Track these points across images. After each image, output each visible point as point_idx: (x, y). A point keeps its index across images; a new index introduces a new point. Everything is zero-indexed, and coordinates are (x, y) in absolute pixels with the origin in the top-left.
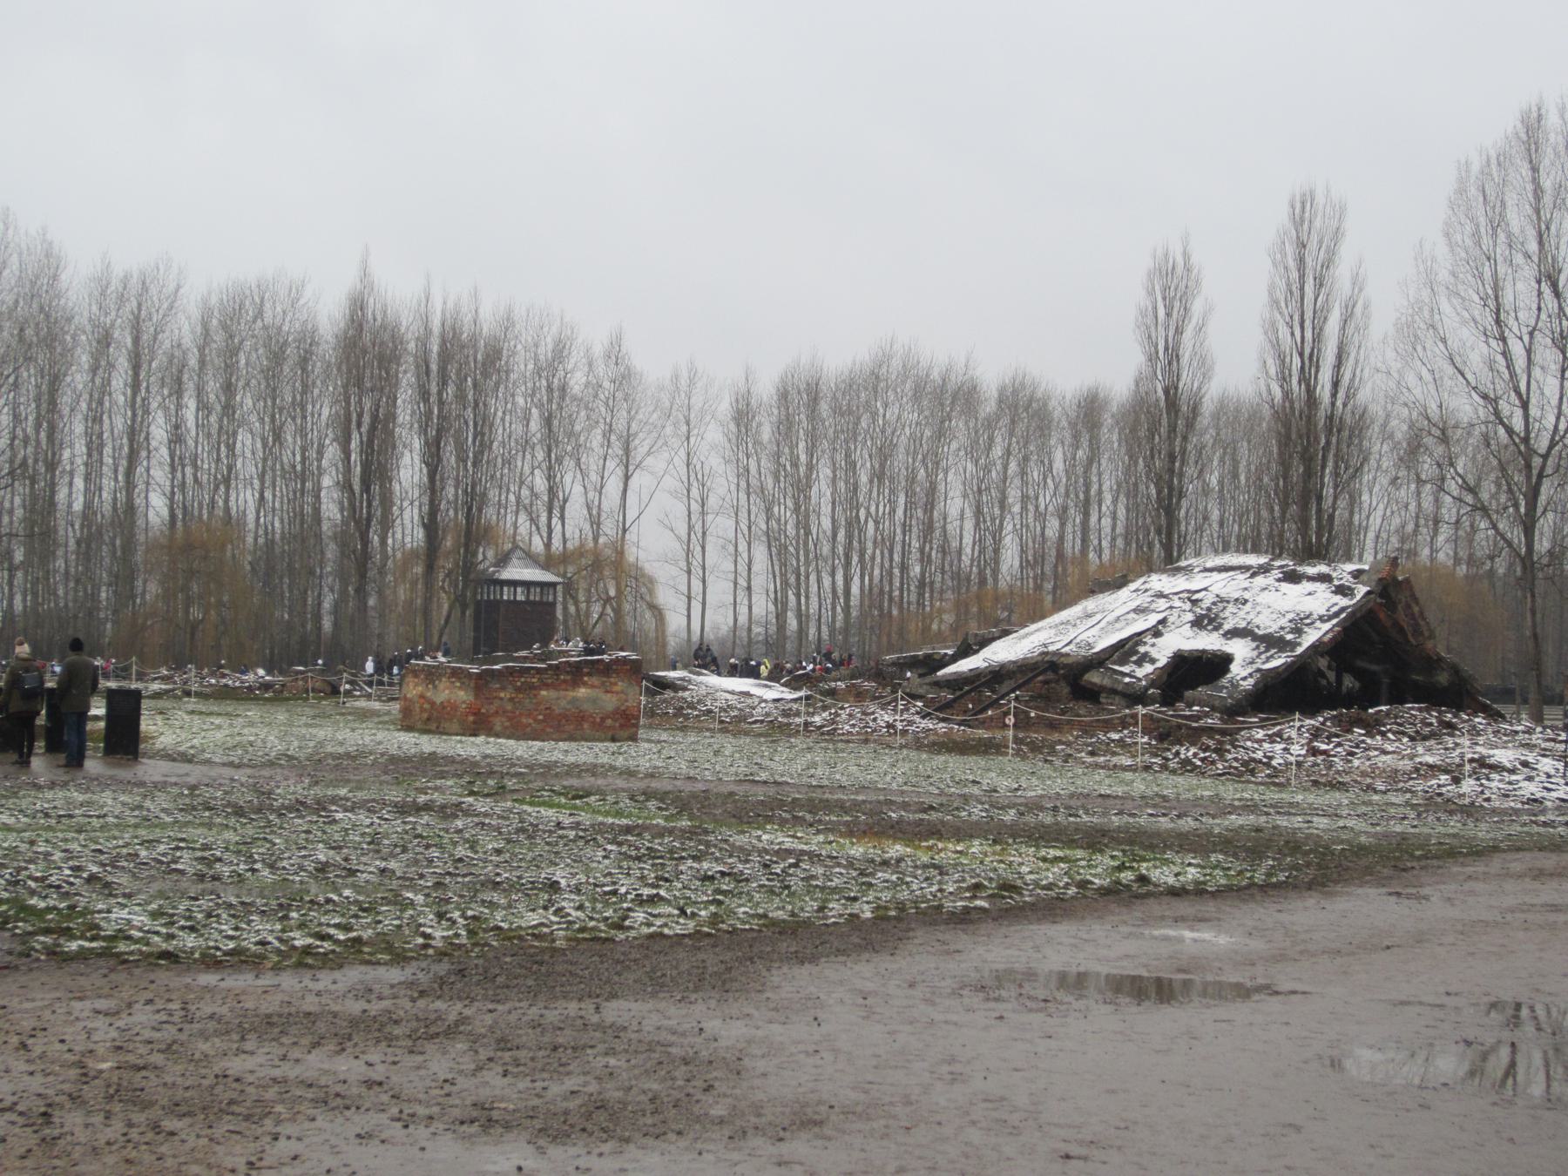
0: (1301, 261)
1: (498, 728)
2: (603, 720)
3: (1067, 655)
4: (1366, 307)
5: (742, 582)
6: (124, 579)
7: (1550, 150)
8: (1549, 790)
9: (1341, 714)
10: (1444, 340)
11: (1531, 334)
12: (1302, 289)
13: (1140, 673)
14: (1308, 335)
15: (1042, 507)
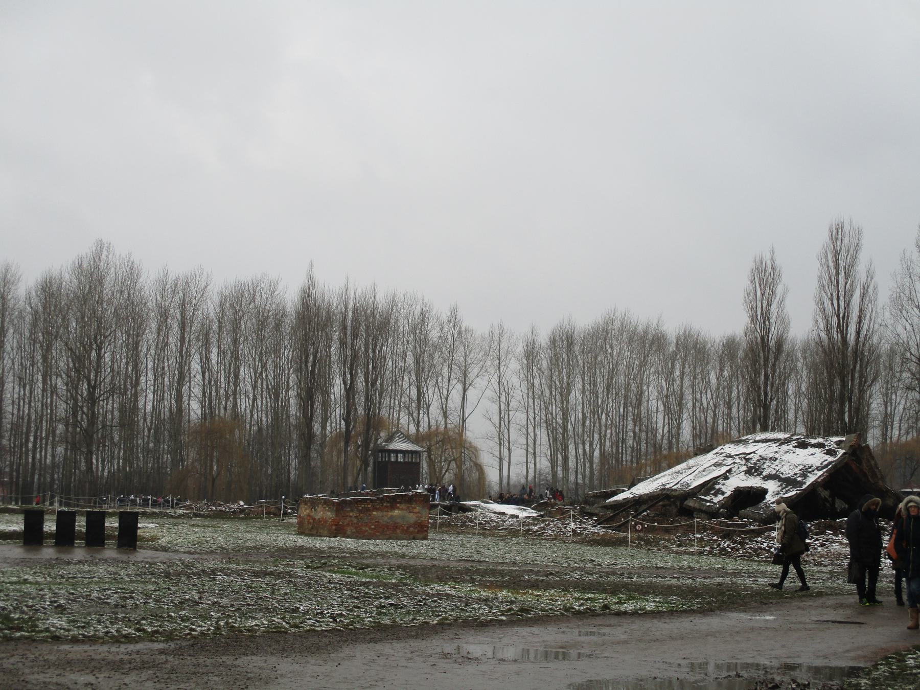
0: (836, 262)
1: (349, 533)
3: (675, 490)
4: (875, 288)
5: (530, 450)
6: (177, 450)
13: (716, 500)
15: (705, 405)
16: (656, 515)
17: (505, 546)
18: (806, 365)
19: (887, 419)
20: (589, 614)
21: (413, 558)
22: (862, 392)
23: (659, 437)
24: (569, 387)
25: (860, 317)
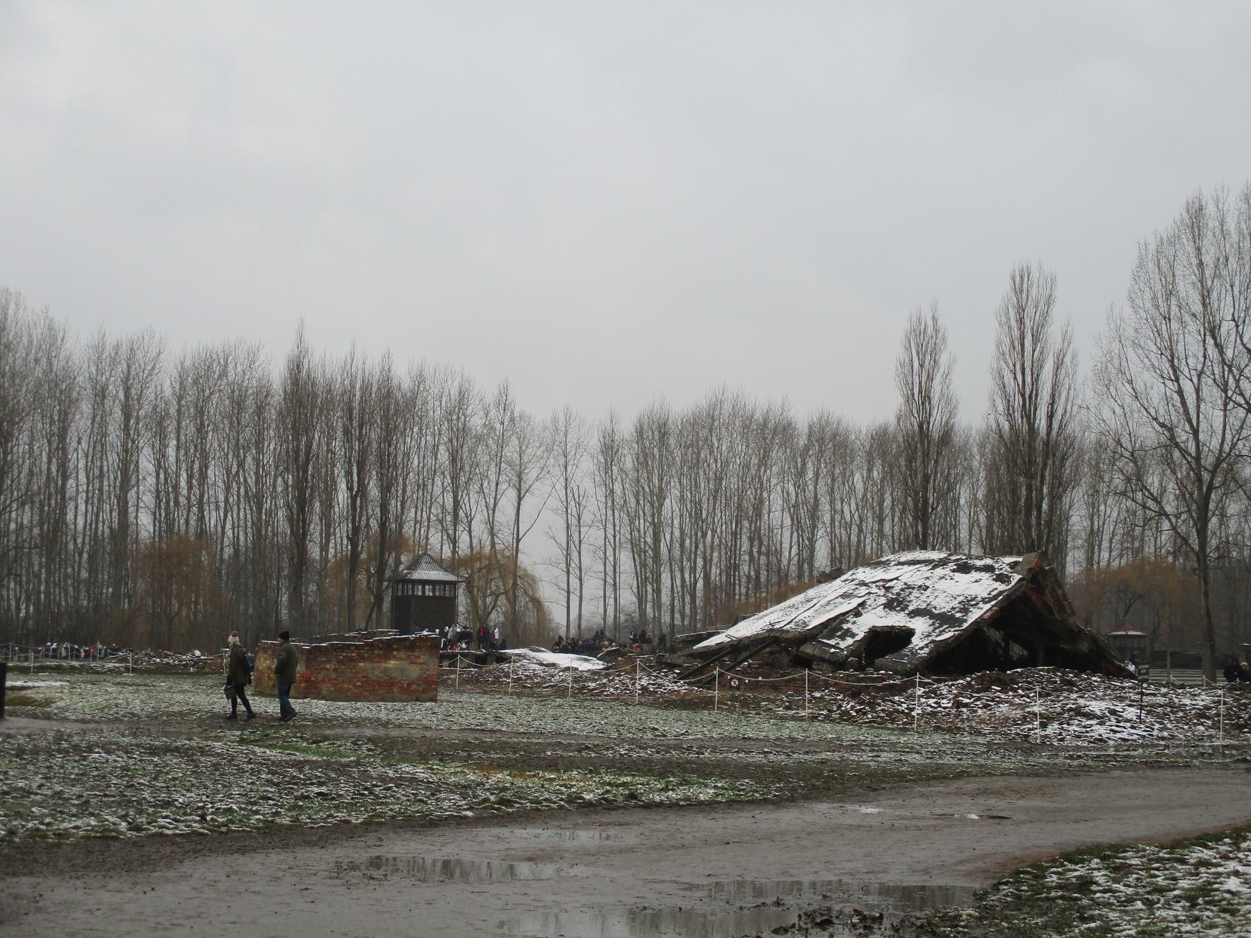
0: (1021, 321)
1: (324, 692)
2: (409, 685)
3: (788, 631)
4: (1074, 357)
5: (610, 580)
7: (1210, 235)
8: (1115, 732)
9: (984, 675)
10: (1130, 382)
11: (1199, 376)
12: (1023, 345)
13: (843, 645)
14: (1028, 379)
16: (761, 666)
17: (540, 710)
18: (985, 464)
19: (1093, 537)
20: (606, 805)
21: (400, 726)
22: (1055, 498)
23: (785, 562)
24: (661, 496)
25: (1053, 396)
